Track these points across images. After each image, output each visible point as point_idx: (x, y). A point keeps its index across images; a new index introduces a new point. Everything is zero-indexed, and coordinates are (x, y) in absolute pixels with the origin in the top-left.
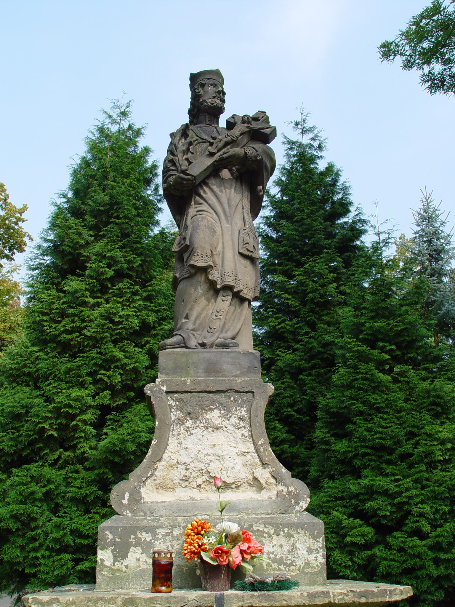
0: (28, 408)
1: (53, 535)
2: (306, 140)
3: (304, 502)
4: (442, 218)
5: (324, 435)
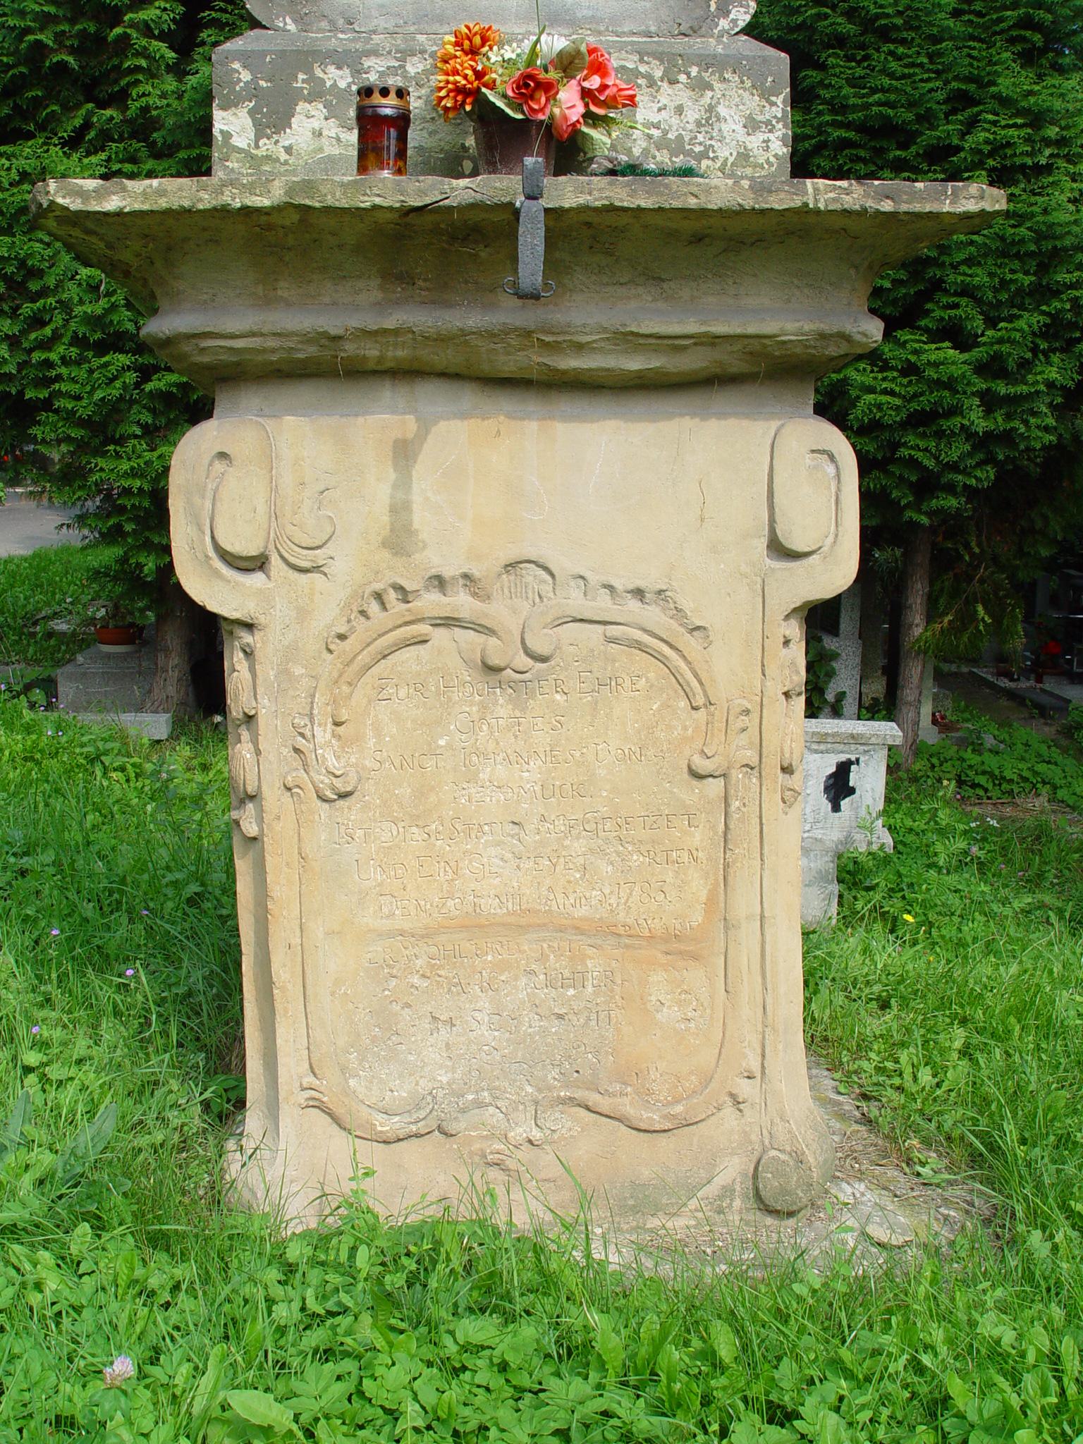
1: (84, 308)
3: (742, 10)
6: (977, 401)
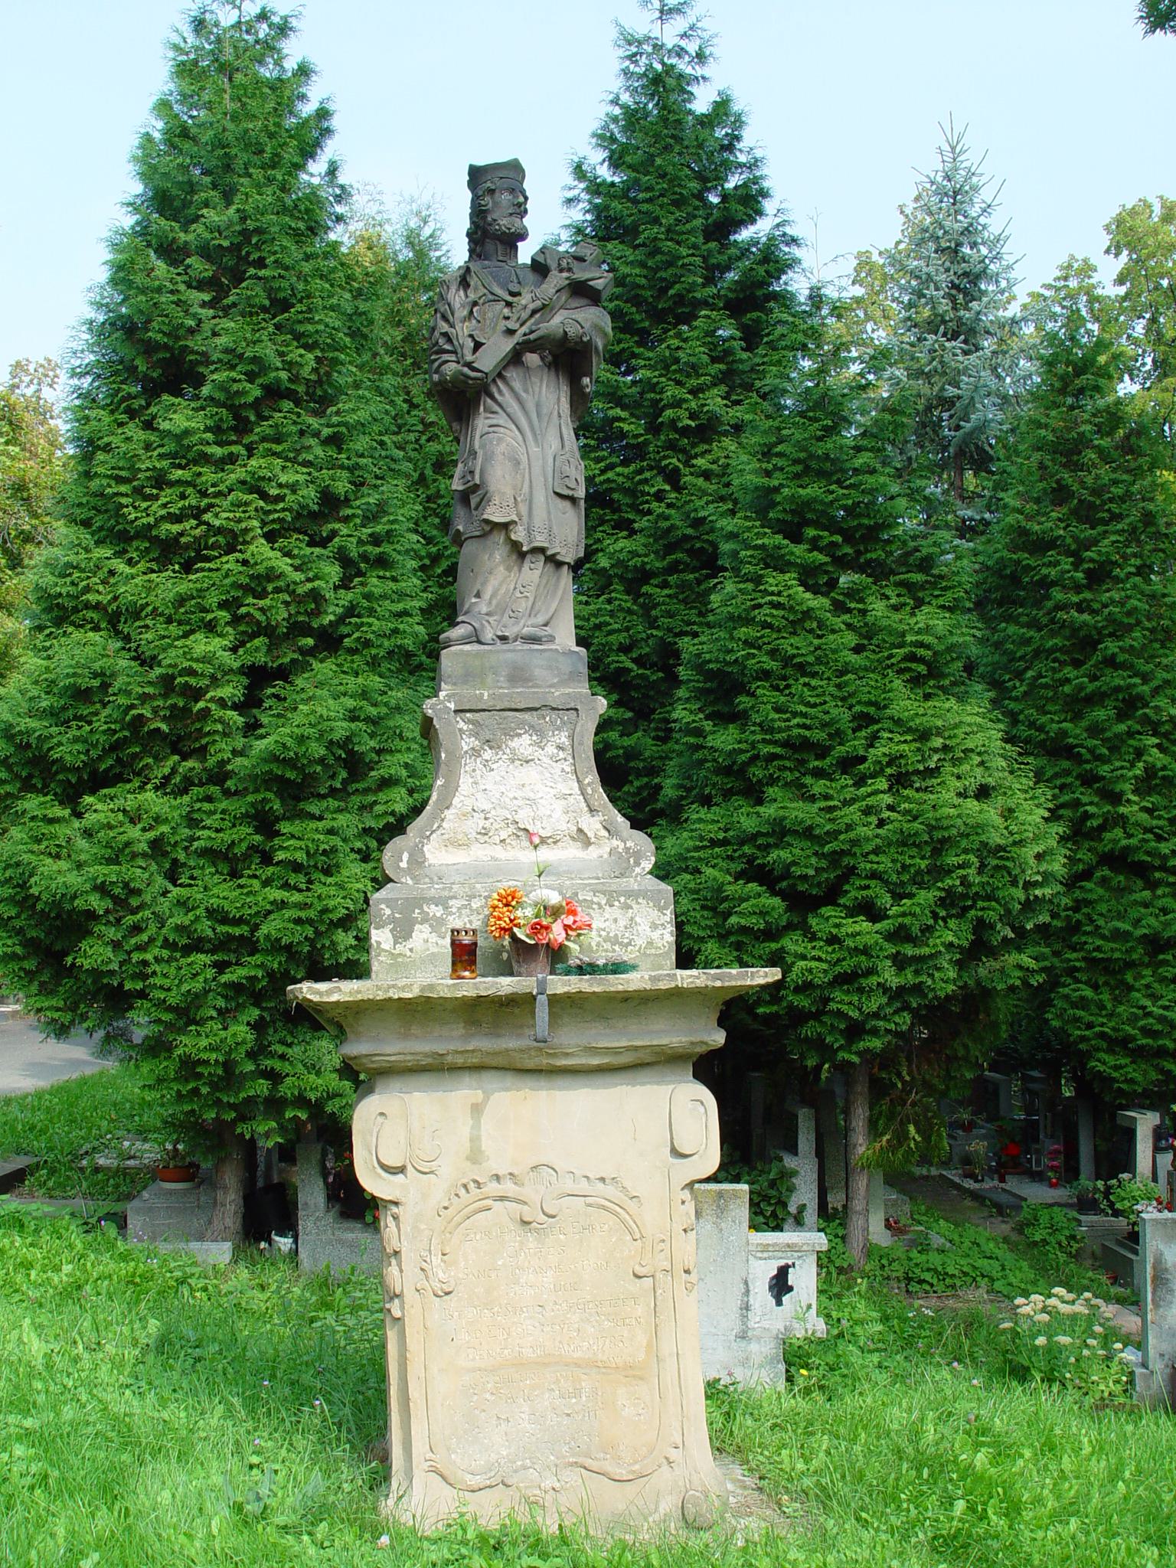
0: (106, 679)
2: (670, 34)
4: (986, 195)
5: (693, 717)
6: (889, 963)
